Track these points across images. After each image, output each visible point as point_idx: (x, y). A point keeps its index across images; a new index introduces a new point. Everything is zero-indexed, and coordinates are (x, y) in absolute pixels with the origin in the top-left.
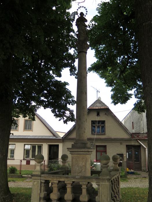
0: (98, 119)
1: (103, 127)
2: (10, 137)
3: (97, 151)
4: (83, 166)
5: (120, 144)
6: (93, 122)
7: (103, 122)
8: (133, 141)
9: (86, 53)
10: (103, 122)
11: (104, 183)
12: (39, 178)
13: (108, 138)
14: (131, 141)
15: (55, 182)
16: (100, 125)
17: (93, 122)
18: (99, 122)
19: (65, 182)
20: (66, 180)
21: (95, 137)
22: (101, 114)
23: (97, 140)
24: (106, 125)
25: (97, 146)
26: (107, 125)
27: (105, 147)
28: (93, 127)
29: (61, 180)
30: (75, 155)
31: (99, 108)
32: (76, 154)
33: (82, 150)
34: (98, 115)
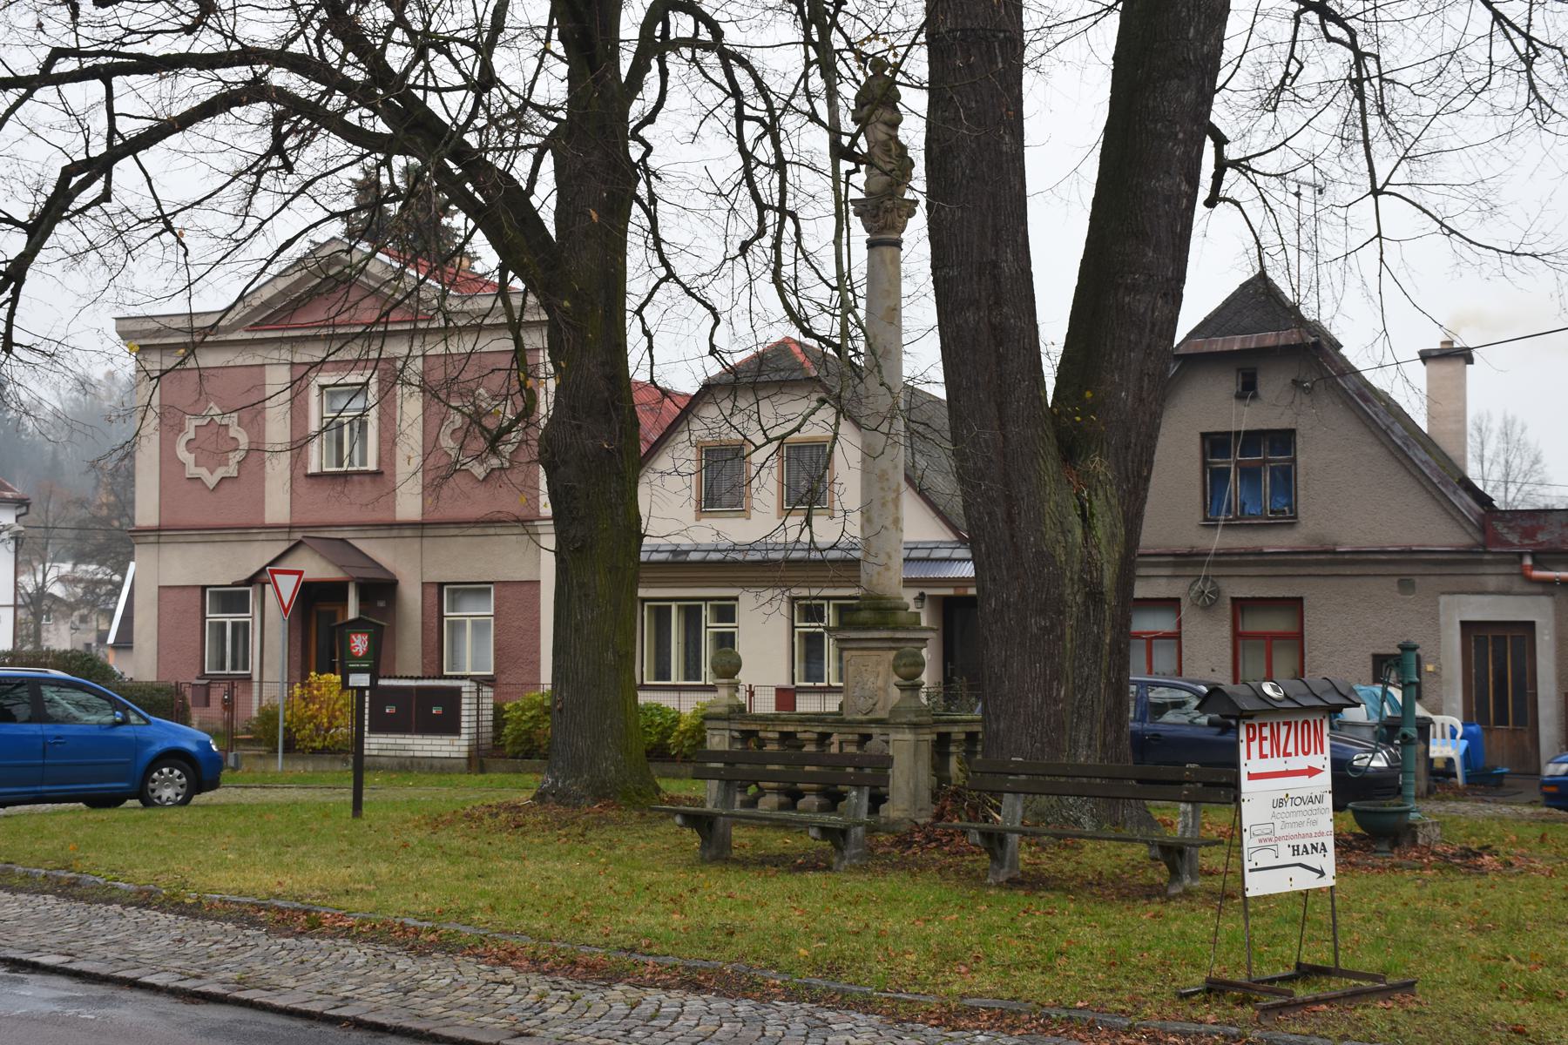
0: (1246, 418)
1: (1286, 479)
2: (366, 752)
3: (1237, 636)
4: (880, 688)
5: (1396, 588)
6: (1215, 444)
7: (1284, 440)
8: (1489, 569)
9: (898, 244)
10: (1284, 440)
11: (899, 737)
12: (725, 724)
13: (1315, 547)
14: (1481, 570)
15: (771, 735)
16: (1265, 461)
17: (1215, 444)
18: (1252, 440)
19: (799, 736)
20: (799, 729)
21: (1218, 540)
22: (1273, 385)
23: (1229, 560)
24: (1301, 459)
25: (1241, 606)
26: (1306, 457)
27: (1296, 604)
28: (1215, 480)
29: (785, 729)
30: (854, 653)
31: (1247, 346)
32: (857, 649)
33: (876, 634)
34: (1248, 390)
